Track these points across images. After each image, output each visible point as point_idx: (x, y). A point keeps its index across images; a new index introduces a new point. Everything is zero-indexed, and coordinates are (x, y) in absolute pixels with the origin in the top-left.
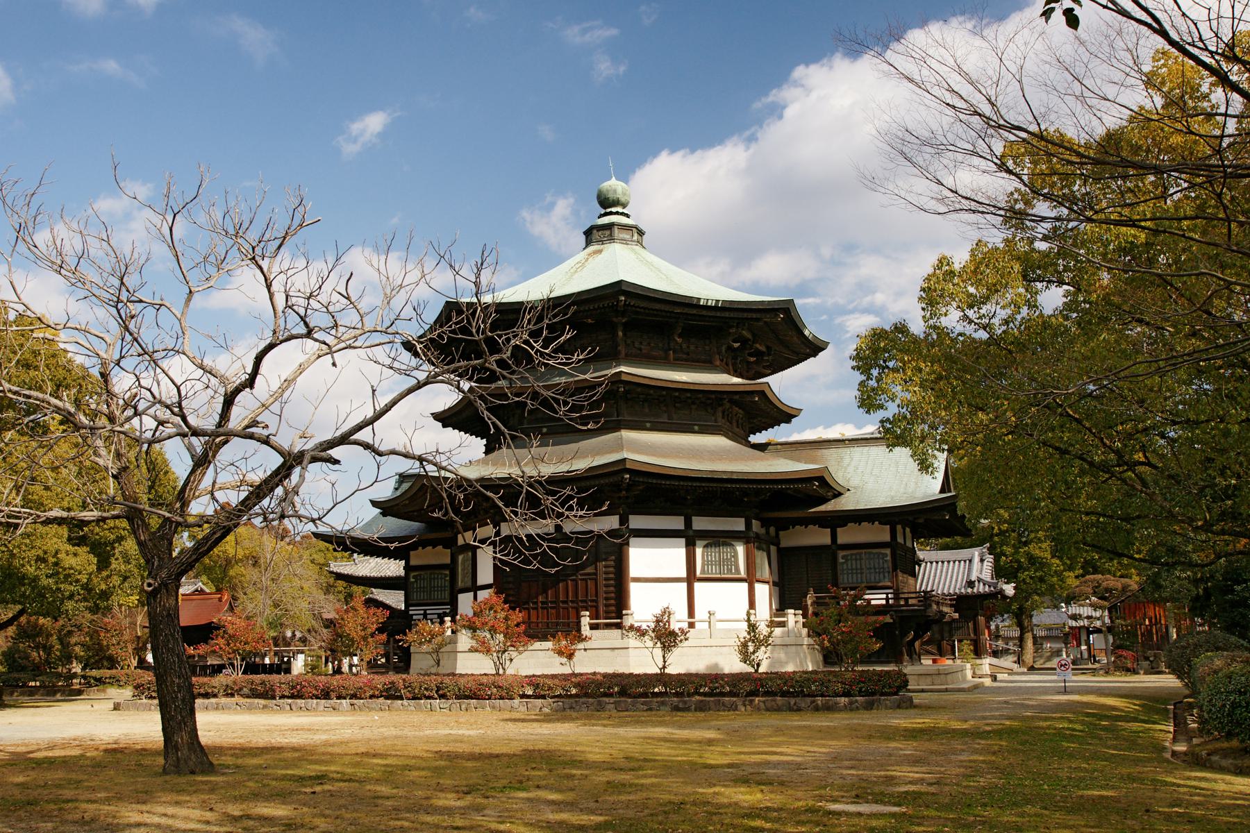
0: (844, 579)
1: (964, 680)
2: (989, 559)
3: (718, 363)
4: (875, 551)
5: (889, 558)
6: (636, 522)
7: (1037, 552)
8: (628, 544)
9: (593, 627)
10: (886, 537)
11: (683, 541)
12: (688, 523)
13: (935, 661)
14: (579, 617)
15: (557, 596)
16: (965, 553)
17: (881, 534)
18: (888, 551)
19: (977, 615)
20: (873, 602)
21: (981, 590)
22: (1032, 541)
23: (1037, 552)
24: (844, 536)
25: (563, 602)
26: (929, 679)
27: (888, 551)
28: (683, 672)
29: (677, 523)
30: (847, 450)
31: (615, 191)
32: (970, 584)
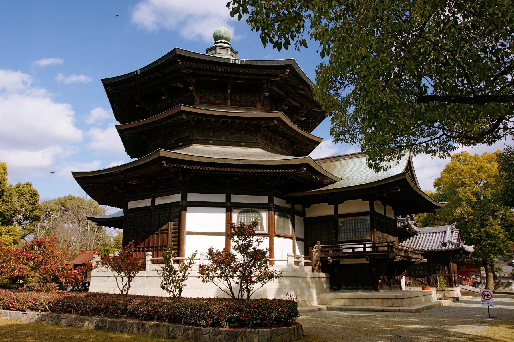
0: (342, 236)
1: (429, 300)
2: (456, 231)
3: (259, 107)
4: (360, 218)
5: (369, 222)
6: (192, 197)
7: (491, 230)
8: (186, 210)
9: (153, 262)
10: (367, 209)
11: (224, 209)
12: (228, 199)
13: (423, 288)
14: (145, 255)
15: (149, 243)
16: (442, 228)
17: (360, 206)
18: (368, 218)
19: (449, 262)
20: (356, 250)
21: (450, 248)
22: (487, 225)
23: (491, 230)
24: (342, 209)
25: (156, 247)
26: (390, 302)
27: (368, 218)
28: (95, 292)
29: (221, 198)
30: (350, 161)
31: (220, 32)
32: (444, 244)
